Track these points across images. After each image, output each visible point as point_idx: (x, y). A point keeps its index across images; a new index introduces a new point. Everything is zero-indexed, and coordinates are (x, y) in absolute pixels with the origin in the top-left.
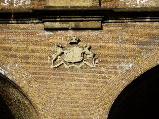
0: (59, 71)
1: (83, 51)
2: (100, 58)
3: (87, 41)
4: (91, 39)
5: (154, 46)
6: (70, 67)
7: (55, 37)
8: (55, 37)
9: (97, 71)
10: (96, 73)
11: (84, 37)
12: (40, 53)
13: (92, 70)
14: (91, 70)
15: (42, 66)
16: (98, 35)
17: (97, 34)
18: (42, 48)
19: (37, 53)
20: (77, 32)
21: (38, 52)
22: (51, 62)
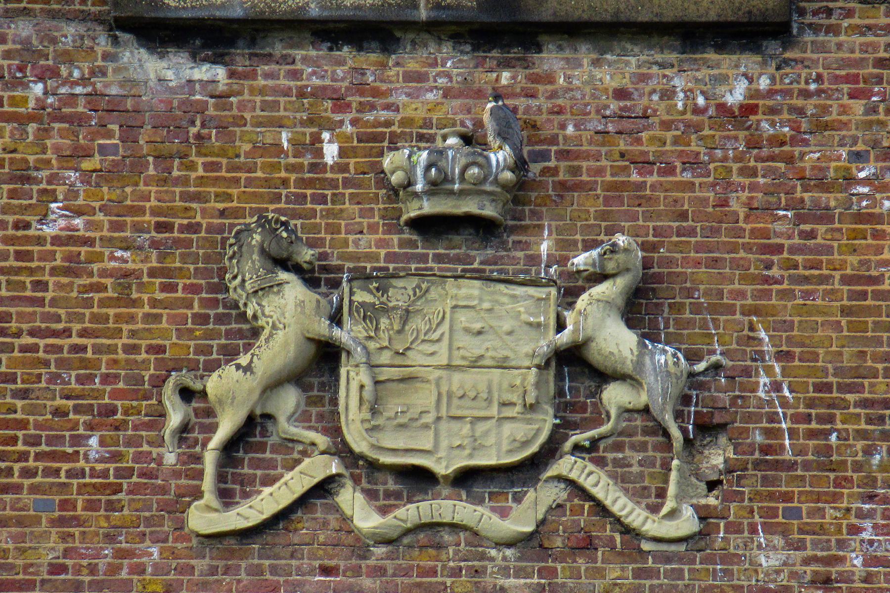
1: (564, 338)
2: (750, 418)
5: (117, 227)
7: (240, 121)
8: (240, 121)
12: (66, 342)
14: (639, 574)
15: (91, 506)
16: (748, 109)
17: (736, 96)
18: (95, 267)
19: (32, 333)
20: (506, 64)
21: (47, 317)
22: (199, 459)
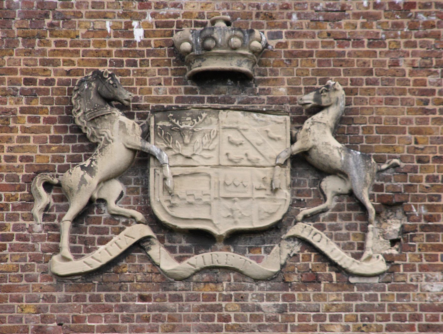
0: (116, 299)
1: (297, 147)
3: (321, 54)
4: (358, 43)
6: (197, 272)
8: (78, 15)
9: (392, 307)
10: (386, 318)
11: (305, 22)
13: (355, 297)
14: (348, 298)
22: (56, 228)
